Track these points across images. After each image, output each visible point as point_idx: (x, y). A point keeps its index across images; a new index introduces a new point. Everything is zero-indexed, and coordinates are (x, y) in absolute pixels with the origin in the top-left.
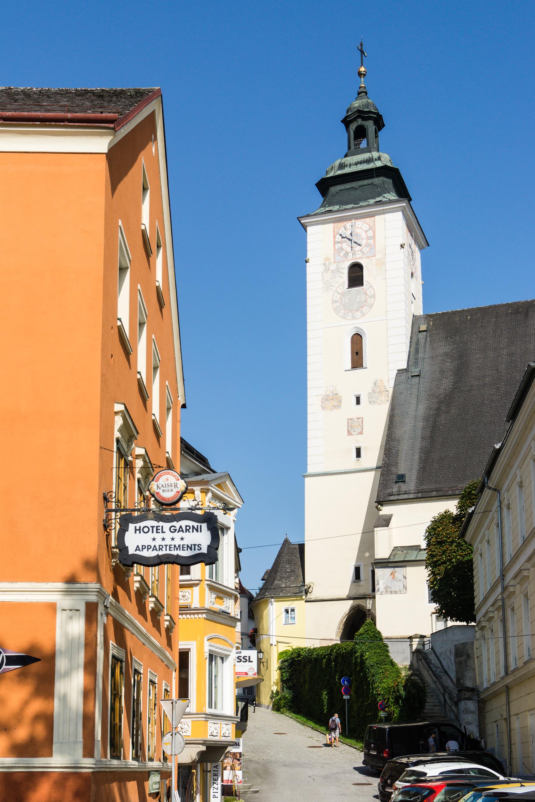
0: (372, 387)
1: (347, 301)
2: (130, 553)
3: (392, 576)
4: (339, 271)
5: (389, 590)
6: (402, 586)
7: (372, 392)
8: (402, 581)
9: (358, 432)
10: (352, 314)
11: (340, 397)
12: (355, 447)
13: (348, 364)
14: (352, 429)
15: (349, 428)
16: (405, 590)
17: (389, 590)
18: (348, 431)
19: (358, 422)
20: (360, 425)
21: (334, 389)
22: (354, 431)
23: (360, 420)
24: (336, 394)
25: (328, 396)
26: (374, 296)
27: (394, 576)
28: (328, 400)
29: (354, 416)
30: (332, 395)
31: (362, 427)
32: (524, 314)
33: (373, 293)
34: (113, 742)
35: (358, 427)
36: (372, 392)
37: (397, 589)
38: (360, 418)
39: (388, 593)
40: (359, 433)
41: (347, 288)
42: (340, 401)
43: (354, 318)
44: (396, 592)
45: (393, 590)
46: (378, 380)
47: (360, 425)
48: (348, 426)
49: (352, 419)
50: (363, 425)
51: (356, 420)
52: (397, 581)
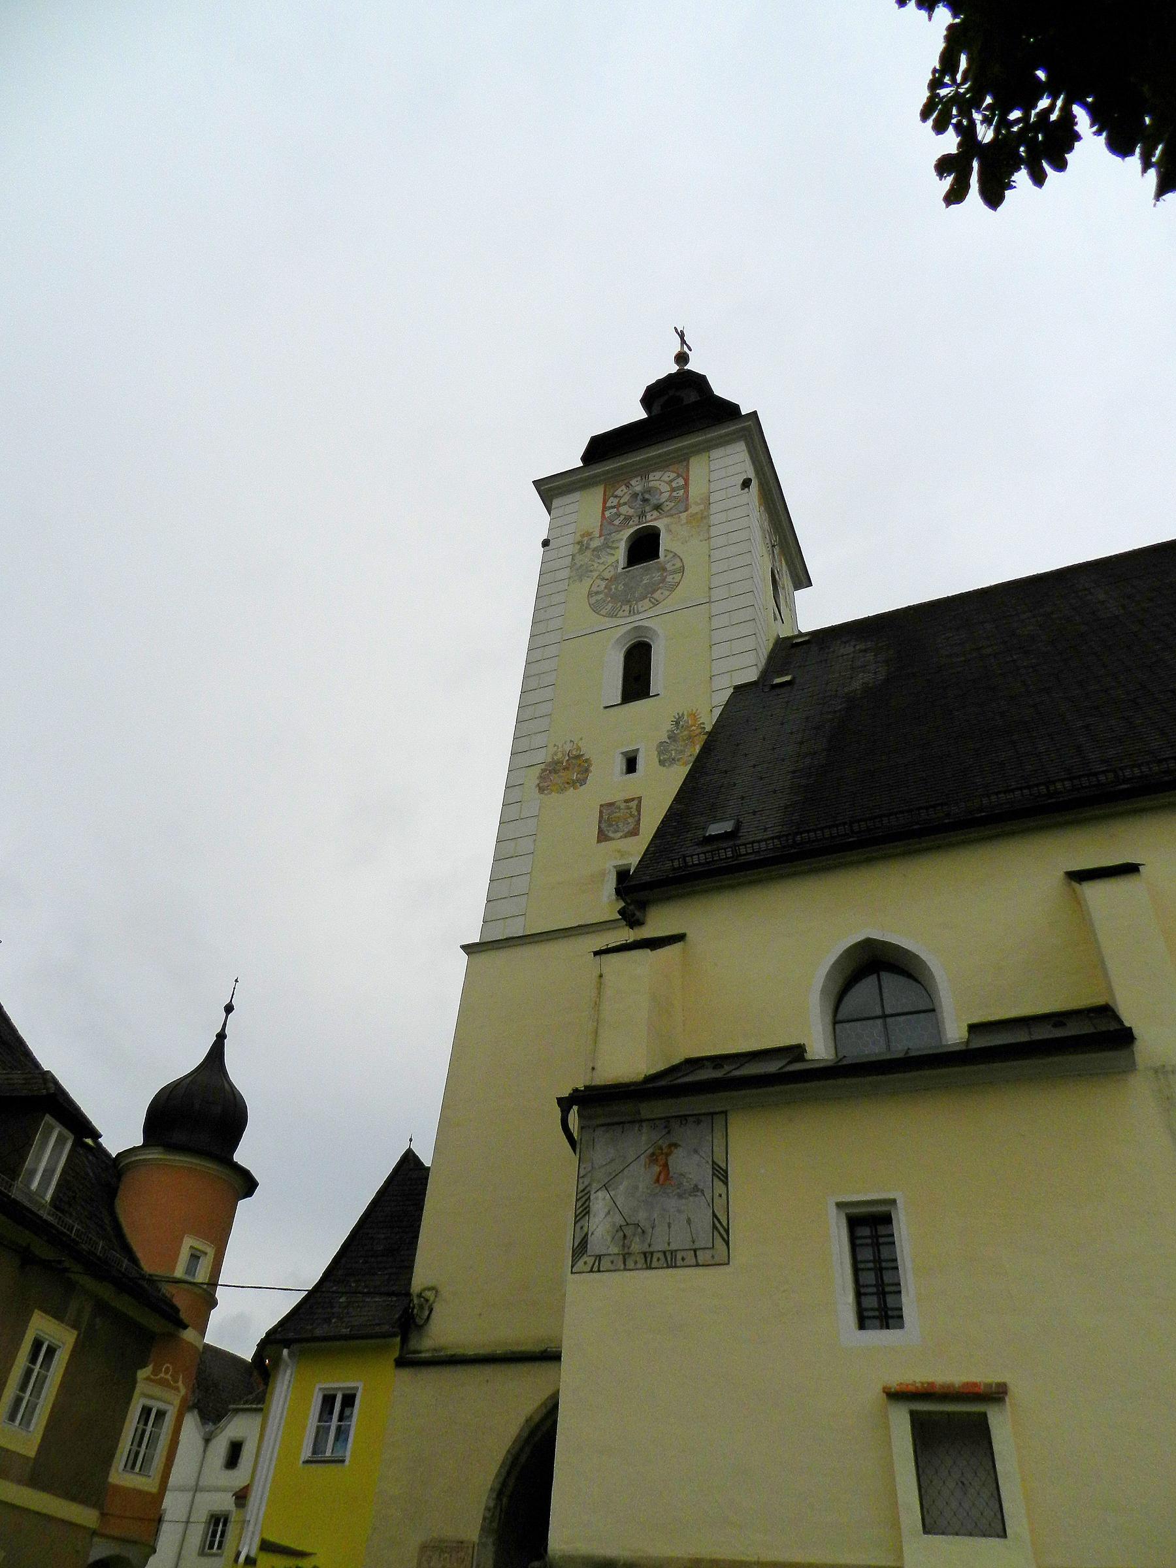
0: (668, 731)
1: (621, 587)
2: (47, 1115)
3: (656, 1169)
4: (609, 547)
5: (636, 1246)
6: (703, 1221)
7: (668, 741)
8: (709, 1196)
9: (626, 830)
10: (630, 607)
11: (587, 761)
12: (615, 867)
13: (614, 690)
14: (610, 825)
15: (603, 826)
16: (719, 1242)
17: (636, 1246)
18: (600, 831)
19: (629, 808)
20: (632, 815)
21: (575, 747)
22: (616, 831)
23: (634, 804)
24: (578, 757)
25: (559, 762)
26: (682, 570)
27: (666, 1165)
28: (556, 772)
29: (618, 796)
30: (568, 760)
31: (637, 818)
32: (707, 1510)
33: (679, 564)
34: (212, 1527)
35: (626, 819)
36: (668, 741)
37: (679, 1240)
38: (633, 800)
39: (630, 1264)
40: (628, 832)
41: (626, 566)
42: (587, 770)
43: (632, 612)
44: (671, 1260)
45: (659, 1245)
46: (685, 713)
47: (632, 815)
48: (600, 822)
49: (611, 804)
50: (639, 814)
51: (623, 806)
52: (680, 1196)
